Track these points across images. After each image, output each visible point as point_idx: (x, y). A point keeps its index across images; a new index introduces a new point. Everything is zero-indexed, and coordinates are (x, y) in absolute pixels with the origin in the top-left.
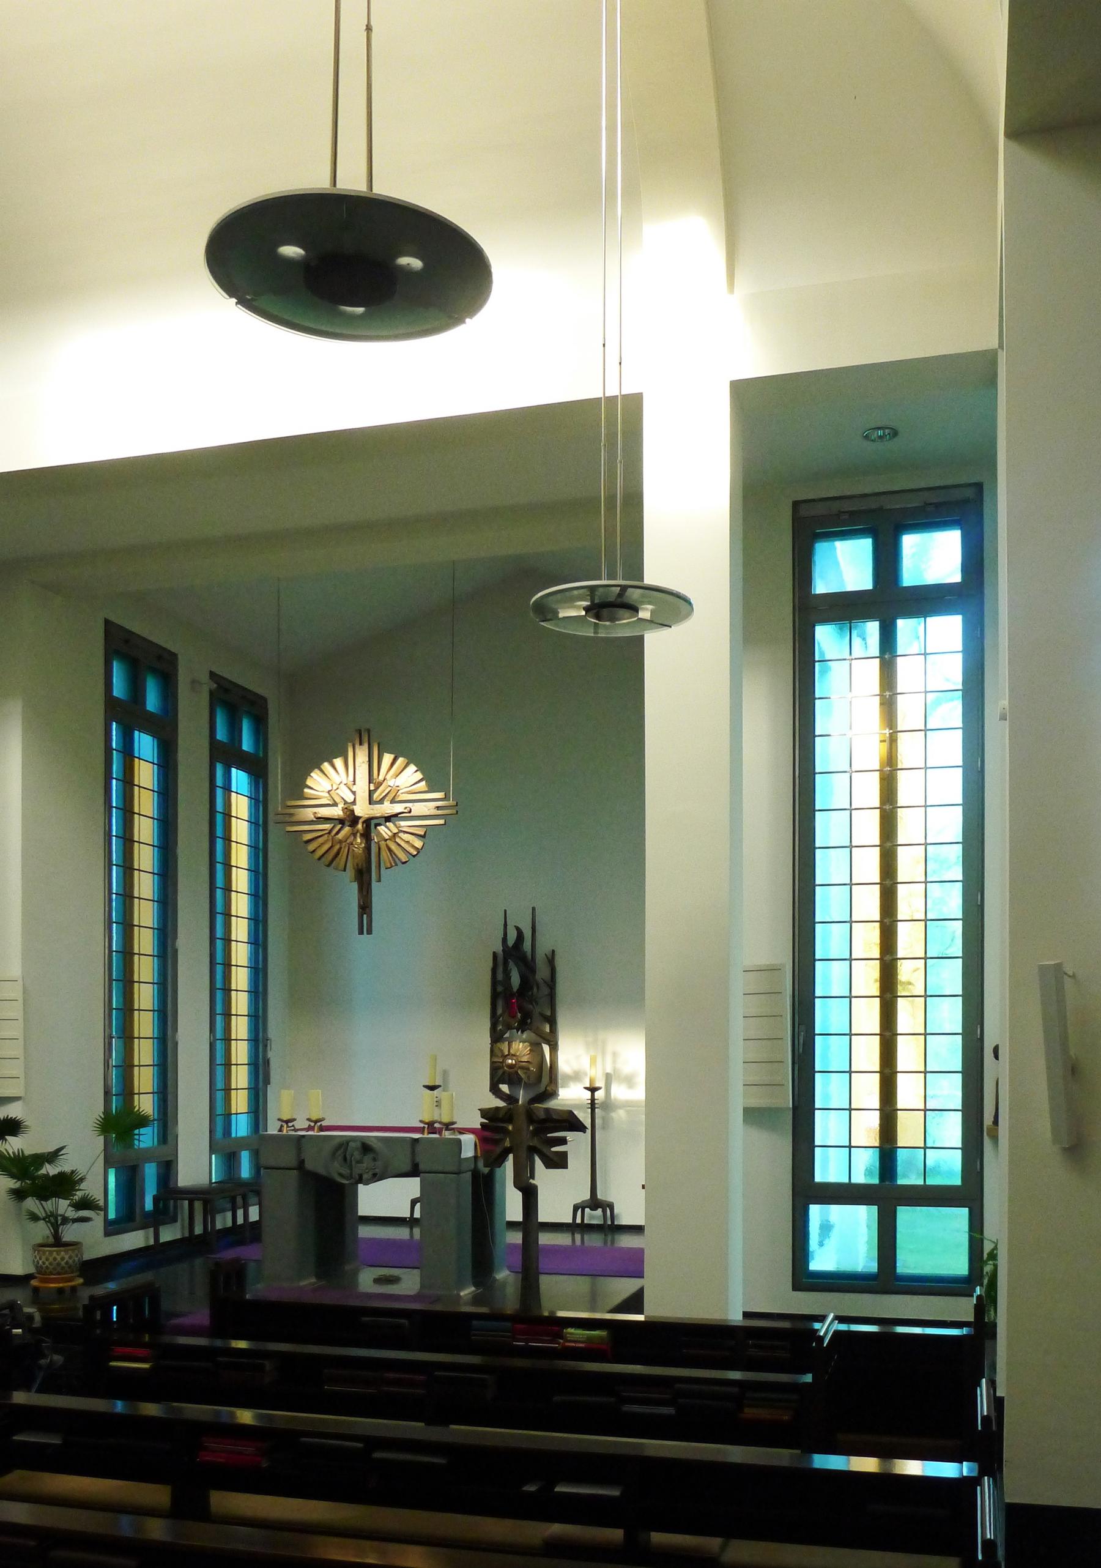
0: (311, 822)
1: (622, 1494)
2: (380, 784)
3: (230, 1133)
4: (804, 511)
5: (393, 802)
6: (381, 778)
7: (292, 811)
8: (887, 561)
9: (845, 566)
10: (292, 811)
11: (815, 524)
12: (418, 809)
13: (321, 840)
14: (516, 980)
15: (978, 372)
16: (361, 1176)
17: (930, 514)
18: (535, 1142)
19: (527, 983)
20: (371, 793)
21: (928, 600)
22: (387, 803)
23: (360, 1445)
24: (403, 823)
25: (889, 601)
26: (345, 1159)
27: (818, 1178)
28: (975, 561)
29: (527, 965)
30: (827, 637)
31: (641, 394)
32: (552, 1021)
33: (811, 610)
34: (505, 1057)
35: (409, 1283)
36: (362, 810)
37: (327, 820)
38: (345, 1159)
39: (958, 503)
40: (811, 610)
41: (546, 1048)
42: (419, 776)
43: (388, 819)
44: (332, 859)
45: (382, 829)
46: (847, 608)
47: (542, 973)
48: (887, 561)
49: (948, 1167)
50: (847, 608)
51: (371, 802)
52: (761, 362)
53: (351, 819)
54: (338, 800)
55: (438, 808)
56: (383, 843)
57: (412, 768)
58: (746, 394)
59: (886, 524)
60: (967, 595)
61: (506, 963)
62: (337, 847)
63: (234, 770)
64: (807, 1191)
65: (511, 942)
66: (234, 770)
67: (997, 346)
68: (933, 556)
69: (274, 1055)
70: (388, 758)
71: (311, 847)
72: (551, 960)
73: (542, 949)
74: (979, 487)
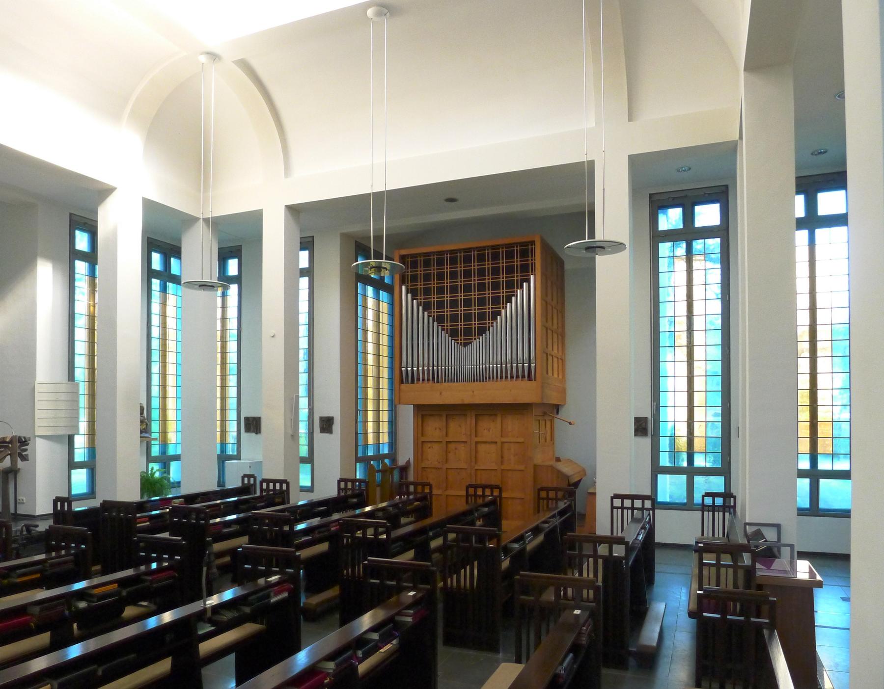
3: (685, 504)
4: (655, 198)
8: (689, 217)
9: (671, 219)
11: (659, 203)
15: (730, 150)
17: (707, 198)
21: (707, 233)
23: (38, 575)
25: (689, 233)
27: (661, 464)
28: (725, 213)
30: (665, 248)
33: (658, 236)
39: (721, 194)
40: (658, 236)
46: (672, 236)
48: (689, 217)
50: (672, 236)
59: (688, 202)
60: (723, 231)
63: (381, 292)
64: (657, 470)
66: (381, 292)
67: (737, 138)
68: (708, 215)
74: (727, 186)
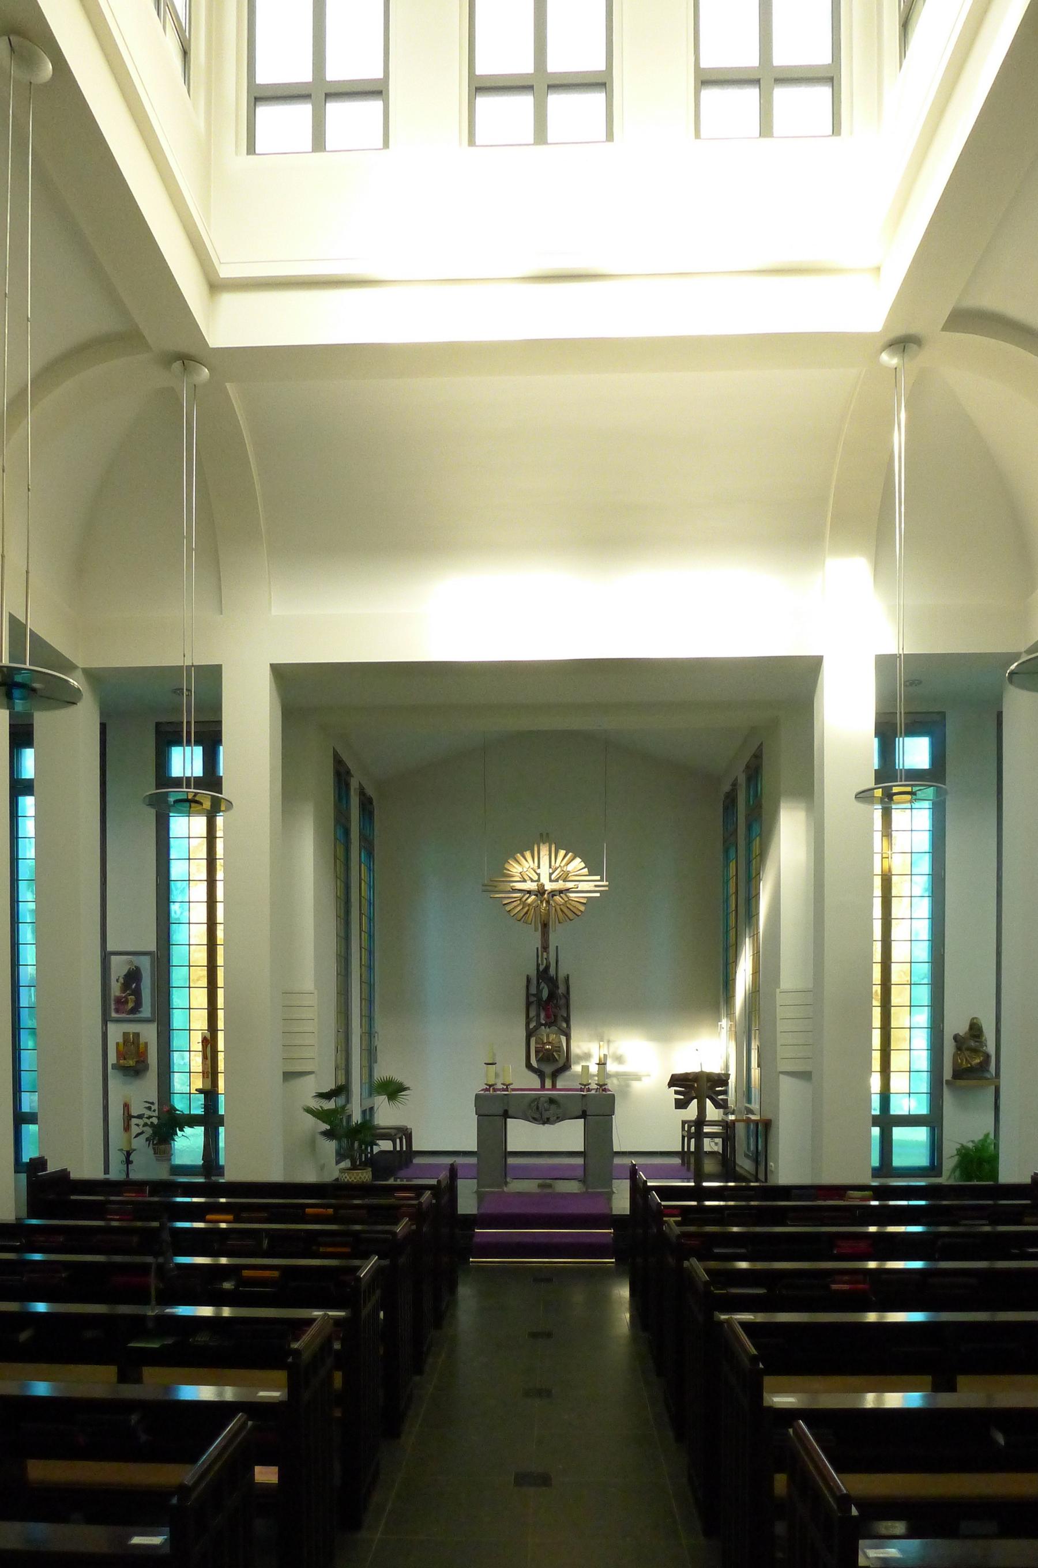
0: (509, 892)
1: (285, 1398)
2: (556, 869)
5: (565, 881)
6: (557, 865)
7: (496, 884)
10: (496, 884)
12: (583, 886)
13: (515, 904)
14: (545, 994)
16: (548, 1119)
18: (710, 1093)
19: (552, 995)
20: (551, 874)
22: (561, 882)
24: (571, 895)
26: (538, 1108)
28: (938, 755)
29: (553, 982)
31: (822, 657)
32: (567, 1020)
34: (544, 1044)
35: (572, 1187)
36: (549, 886)
37: (520, 891)
38: (538, 1108)
41: (563, 1039)
42: (583, 865)
43: (561, 892)
44: (523, 919)
45: (557, 898)
47: (562, 990)
49: (920, 1106)
51: (551, 880)
52: (891, 648)
53: (541, 892)
54: (527, 878)
55: (596, 886)
56: (558, 908)
57: (578, 860)
58: (885, 664)
61: (538, 983)
62: (526, 910)
65: (541, 968)
69: (378, 1043)
70: (562, 853)
71: (508, 908)
72: (567, 979)
73: (561, 975)
